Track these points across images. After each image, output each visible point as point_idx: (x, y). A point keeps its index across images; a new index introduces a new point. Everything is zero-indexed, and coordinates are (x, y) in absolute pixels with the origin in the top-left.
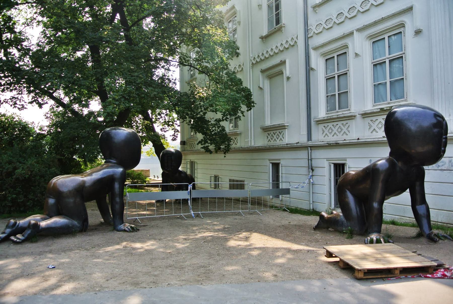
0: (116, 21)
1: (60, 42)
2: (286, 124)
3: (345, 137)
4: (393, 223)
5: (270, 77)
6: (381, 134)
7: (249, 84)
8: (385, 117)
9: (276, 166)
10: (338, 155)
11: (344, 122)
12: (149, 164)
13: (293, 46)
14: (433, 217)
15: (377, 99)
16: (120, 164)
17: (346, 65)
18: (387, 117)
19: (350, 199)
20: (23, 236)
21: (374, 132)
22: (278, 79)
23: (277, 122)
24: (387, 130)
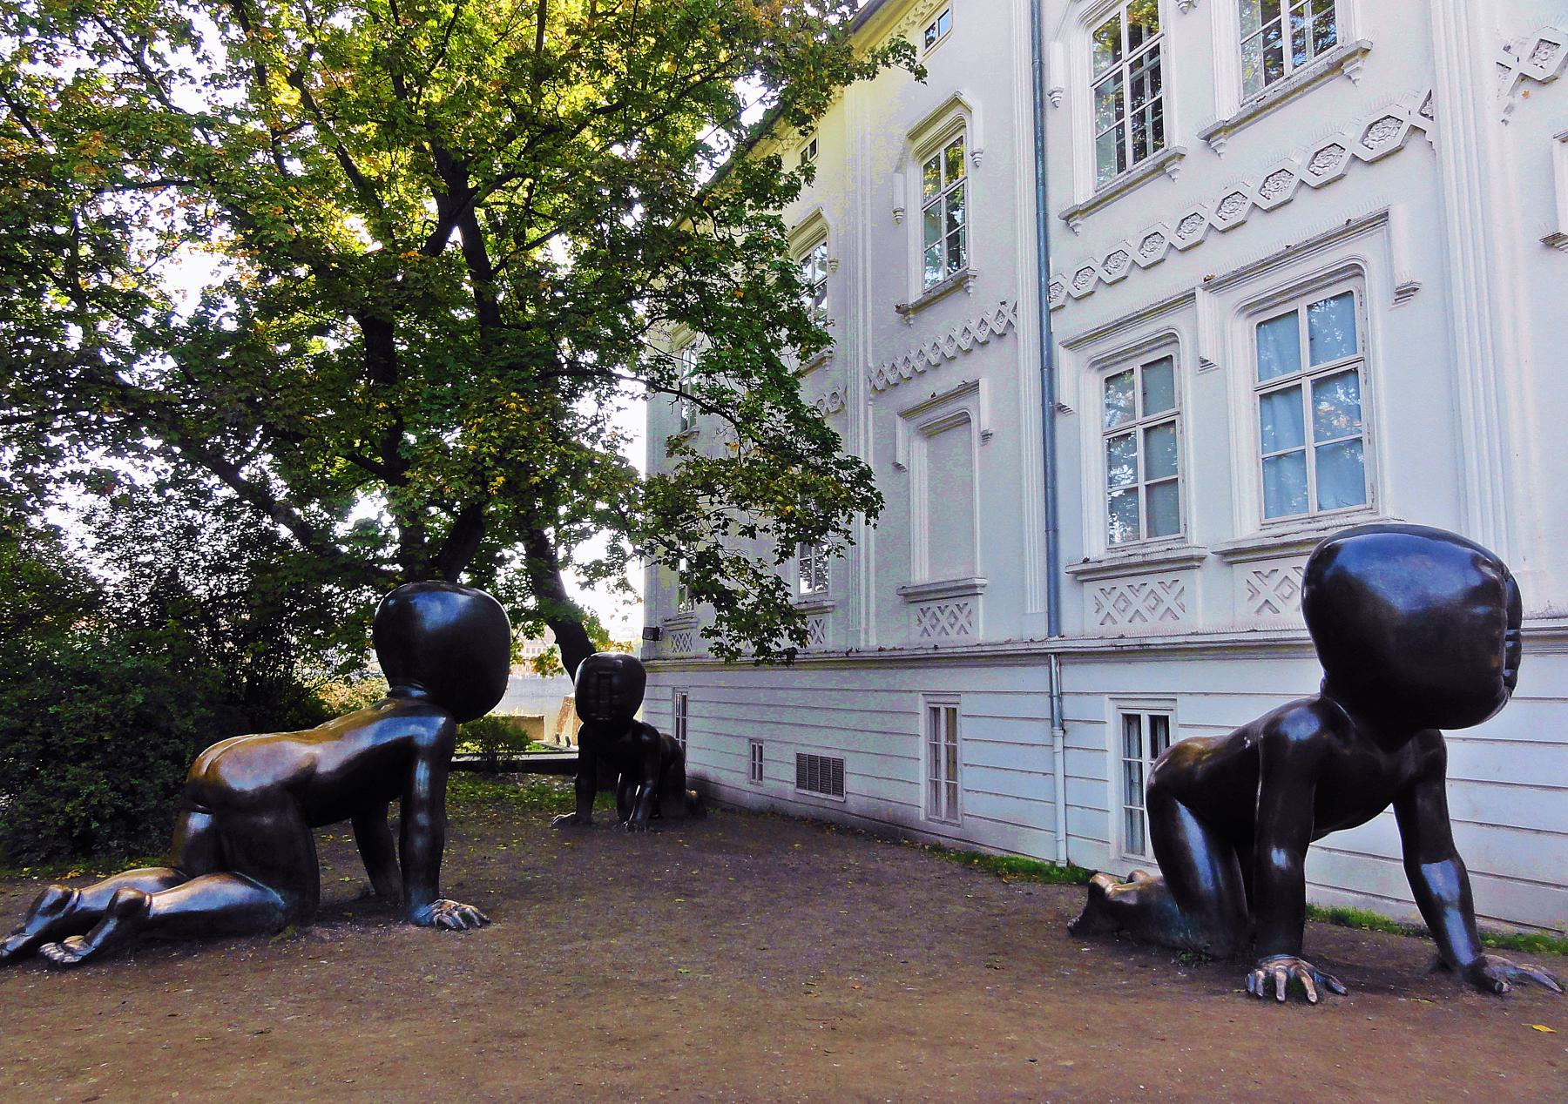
0: (449, 247)
1: (272, 305)
2: (977, 582)
3: (1169, 625)
4: (1339, 918)
5: (930, 432)
6: (1293, 620)
7: (862, 448)
8: (1304, 562)
9: (945, 717)
10: (1144, 682)
11: (1168, 578)
12: (538, 700)
13: (1002, 335)
14: (1481, 903)
15: (1277, 498)
16: (436, 703)
17: (1170, 396)
18: (1312, 563)
19: (1193, 832)
20: (88, 941)
21: (1266, 610)
22: (956, 437)
23: (954, 573)
24: (1315, 609)
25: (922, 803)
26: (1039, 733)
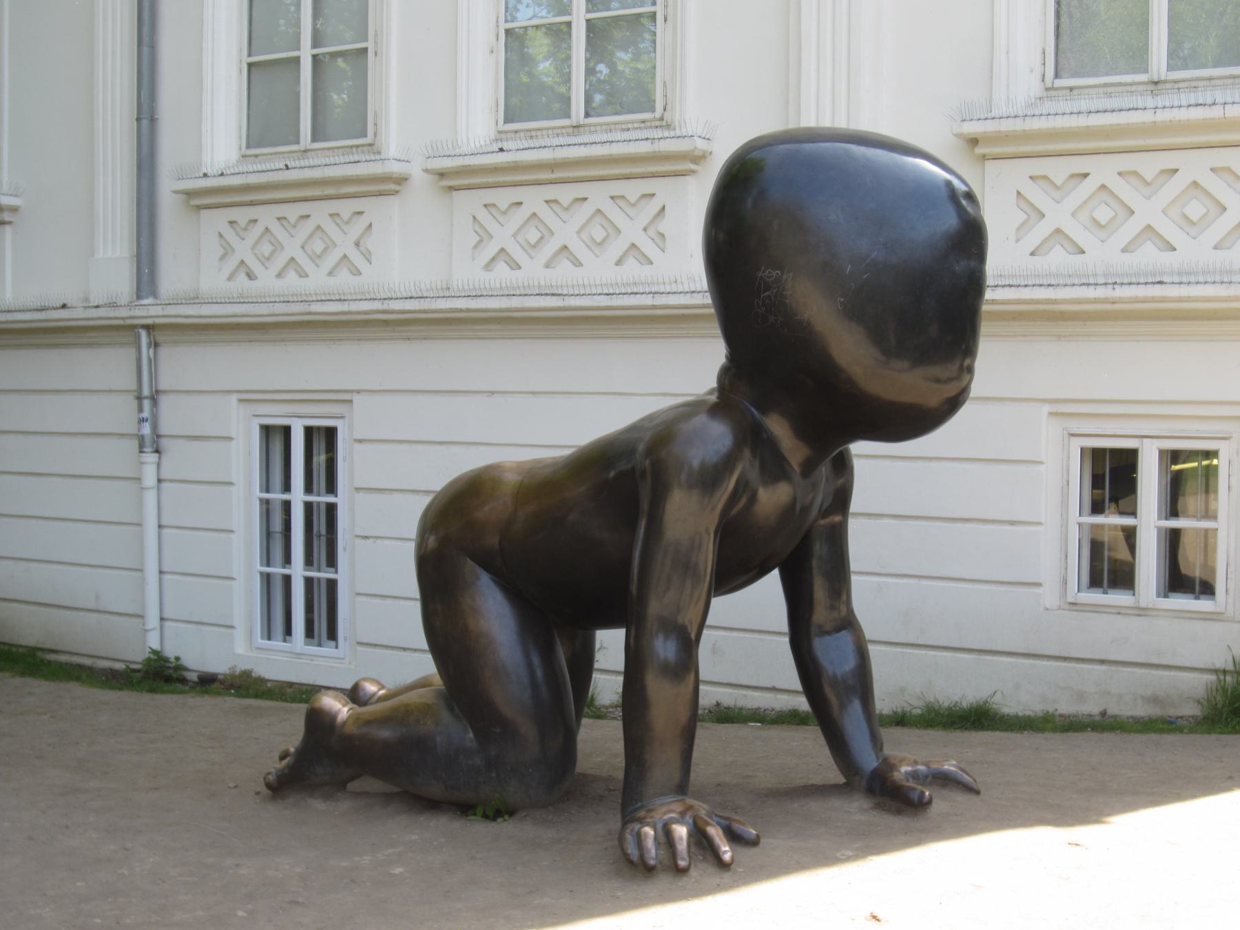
6: (683, 269)
21: (631, 262)
25: (238, 619)
26: (119, 456)
